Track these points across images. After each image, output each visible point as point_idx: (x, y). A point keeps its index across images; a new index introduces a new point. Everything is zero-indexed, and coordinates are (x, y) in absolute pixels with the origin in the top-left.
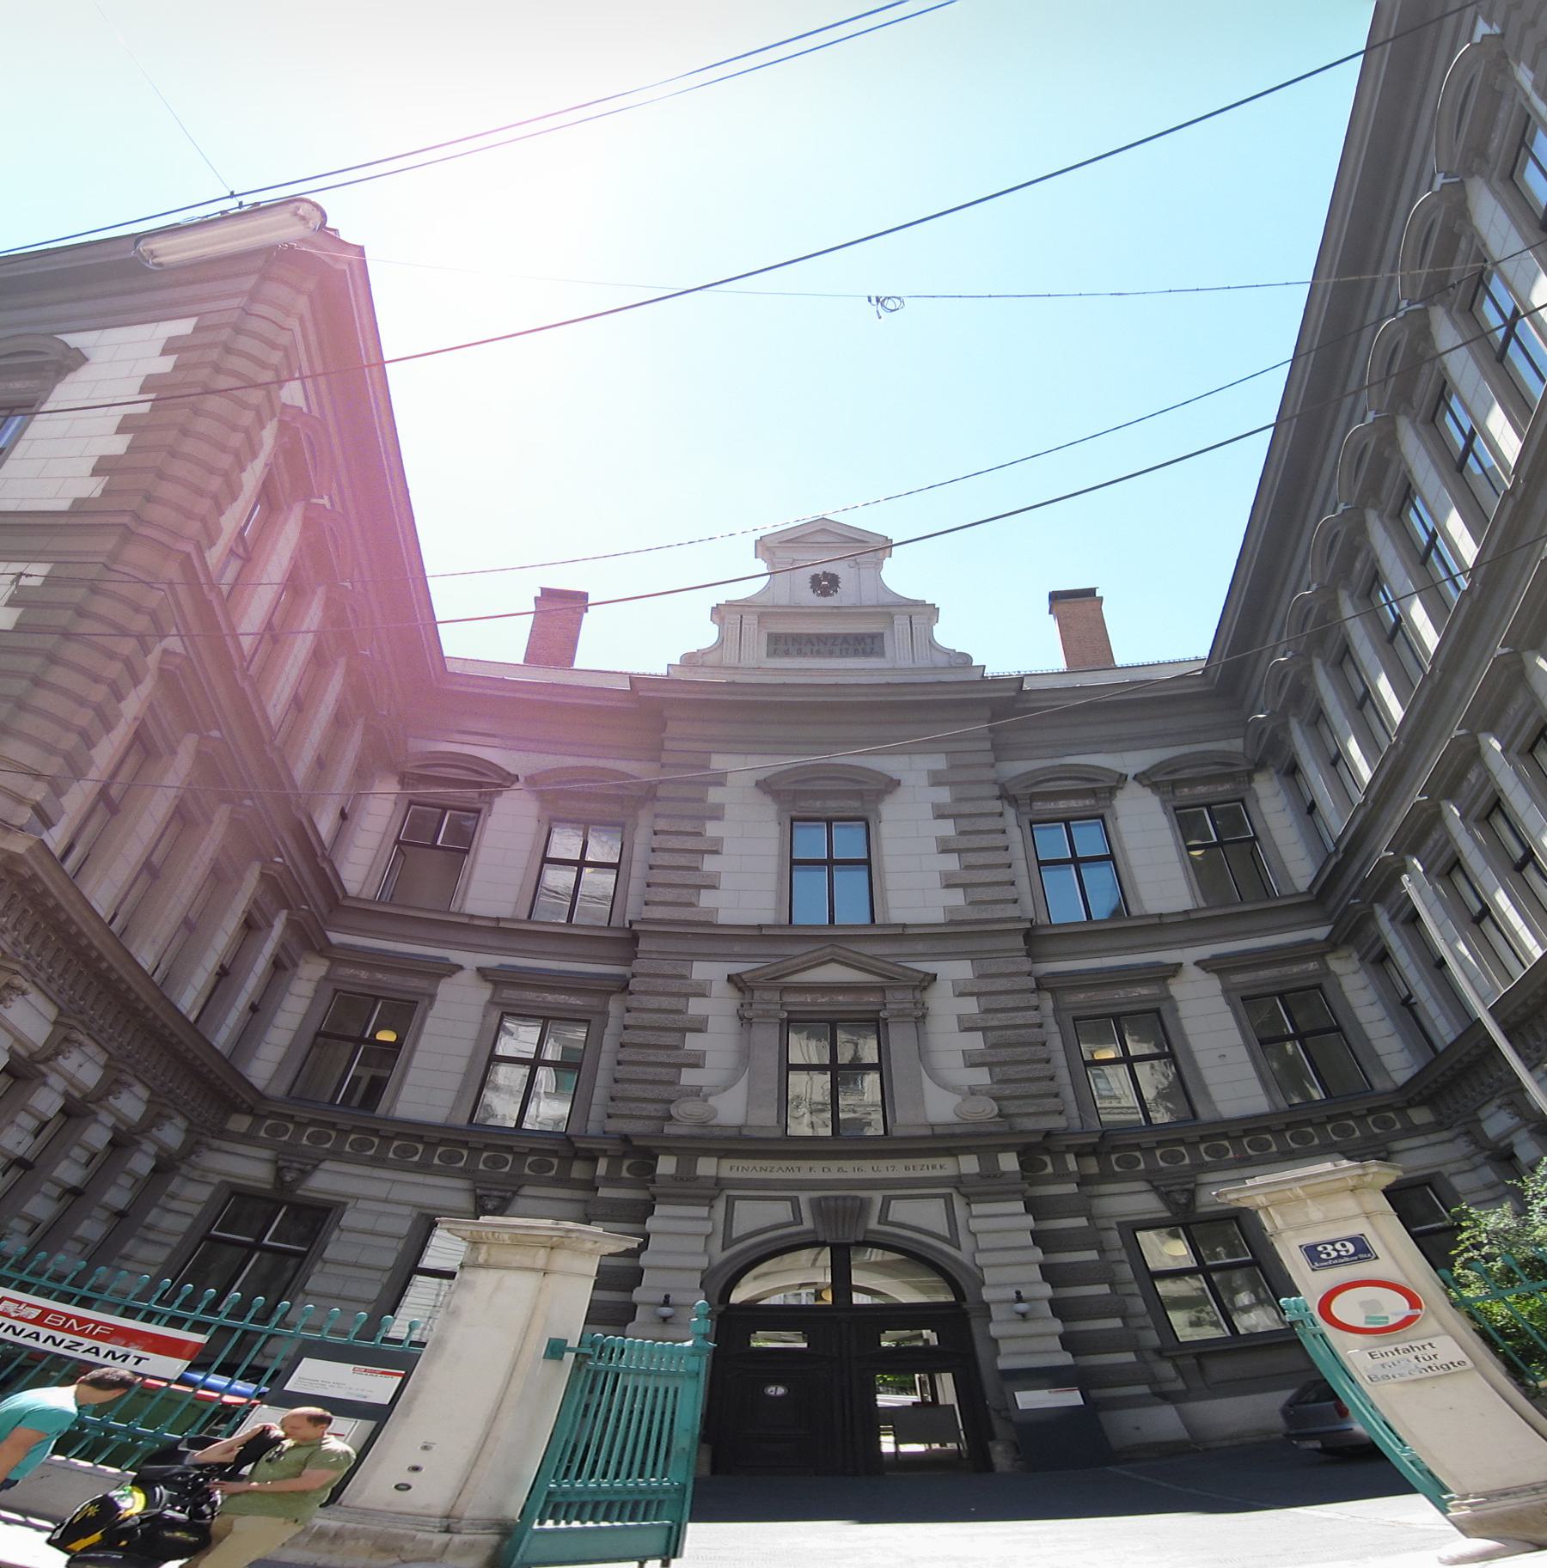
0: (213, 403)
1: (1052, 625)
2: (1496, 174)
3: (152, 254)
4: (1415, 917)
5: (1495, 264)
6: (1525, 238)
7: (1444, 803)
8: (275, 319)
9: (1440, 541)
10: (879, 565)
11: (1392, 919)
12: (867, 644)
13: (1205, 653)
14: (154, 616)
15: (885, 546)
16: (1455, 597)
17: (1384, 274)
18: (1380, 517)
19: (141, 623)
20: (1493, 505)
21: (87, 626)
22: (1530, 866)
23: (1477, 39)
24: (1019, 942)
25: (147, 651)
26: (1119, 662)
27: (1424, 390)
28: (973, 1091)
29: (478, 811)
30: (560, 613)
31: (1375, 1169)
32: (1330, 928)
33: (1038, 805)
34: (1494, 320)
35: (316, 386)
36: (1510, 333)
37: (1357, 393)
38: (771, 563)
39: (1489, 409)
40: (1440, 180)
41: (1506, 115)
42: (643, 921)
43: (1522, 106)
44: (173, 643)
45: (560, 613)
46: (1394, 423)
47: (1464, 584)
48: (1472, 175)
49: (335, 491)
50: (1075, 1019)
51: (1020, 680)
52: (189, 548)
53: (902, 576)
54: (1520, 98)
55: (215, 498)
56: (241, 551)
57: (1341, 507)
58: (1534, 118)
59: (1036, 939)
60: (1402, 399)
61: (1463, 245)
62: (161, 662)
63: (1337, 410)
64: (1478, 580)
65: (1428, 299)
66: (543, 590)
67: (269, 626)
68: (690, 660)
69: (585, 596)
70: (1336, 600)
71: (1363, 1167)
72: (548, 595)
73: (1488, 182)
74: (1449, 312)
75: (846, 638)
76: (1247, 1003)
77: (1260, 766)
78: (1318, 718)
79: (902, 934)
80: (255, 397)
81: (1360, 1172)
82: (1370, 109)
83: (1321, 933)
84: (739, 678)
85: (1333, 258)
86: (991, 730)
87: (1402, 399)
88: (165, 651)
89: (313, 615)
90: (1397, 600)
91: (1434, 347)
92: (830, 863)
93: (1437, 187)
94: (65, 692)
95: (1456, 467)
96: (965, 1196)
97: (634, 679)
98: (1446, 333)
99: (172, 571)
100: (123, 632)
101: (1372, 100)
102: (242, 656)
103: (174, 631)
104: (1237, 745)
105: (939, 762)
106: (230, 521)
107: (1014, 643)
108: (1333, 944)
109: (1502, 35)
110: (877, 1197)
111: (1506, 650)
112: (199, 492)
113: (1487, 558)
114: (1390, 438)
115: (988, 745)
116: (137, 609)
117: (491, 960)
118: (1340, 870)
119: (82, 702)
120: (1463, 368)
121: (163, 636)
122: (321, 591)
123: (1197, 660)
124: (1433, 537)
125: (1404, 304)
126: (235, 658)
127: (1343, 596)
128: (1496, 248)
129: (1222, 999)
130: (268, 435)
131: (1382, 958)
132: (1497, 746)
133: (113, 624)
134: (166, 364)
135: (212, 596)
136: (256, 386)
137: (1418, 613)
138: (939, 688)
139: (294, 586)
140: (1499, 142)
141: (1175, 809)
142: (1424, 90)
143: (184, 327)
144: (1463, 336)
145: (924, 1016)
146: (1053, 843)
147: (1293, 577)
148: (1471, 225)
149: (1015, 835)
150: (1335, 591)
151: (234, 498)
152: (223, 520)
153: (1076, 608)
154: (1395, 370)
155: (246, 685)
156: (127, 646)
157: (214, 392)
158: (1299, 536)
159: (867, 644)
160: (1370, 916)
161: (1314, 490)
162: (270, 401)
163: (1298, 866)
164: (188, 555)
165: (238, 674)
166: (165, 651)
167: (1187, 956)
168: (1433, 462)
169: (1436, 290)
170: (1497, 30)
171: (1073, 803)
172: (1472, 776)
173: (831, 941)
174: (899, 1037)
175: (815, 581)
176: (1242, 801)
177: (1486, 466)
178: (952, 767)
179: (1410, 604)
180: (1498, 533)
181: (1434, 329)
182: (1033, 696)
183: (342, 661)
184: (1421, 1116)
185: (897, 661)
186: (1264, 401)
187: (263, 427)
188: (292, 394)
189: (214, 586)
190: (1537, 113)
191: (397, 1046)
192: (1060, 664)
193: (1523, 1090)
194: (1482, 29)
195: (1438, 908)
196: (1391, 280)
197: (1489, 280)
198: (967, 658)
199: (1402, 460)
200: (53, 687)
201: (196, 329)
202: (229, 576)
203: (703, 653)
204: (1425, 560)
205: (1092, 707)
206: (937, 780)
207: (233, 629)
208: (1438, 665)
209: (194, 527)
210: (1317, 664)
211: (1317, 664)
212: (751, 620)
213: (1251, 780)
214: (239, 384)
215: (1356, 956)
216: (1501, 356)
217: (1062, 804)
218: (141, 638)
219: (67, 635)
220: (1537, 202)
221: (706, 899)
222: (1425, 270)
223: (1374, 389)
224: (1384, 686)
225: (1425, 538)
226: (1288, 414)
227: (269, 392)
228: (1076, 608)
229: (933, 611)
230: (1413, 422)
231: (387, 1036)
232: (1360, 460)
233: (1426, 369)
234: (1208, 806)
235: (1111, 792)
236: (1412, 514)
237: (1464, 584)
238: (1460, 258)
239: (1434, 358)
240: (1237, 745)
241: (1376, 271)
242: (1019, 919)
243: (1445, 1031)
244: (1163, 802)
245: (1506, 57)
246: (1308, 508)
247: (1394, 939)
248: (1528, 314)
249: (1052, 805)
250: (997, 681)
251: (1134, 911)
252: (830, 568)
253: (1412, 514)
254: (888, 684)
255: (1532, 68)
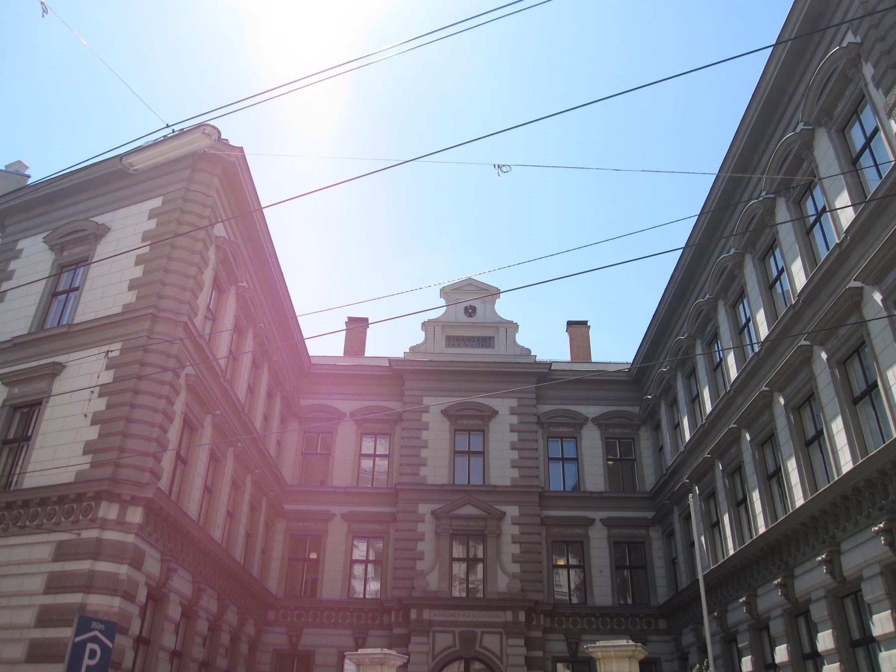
0: (180, 241)
1: (566, 338)
2: (835, 127)
3: (131, 165)
4: (689, 517)
5: (820, 179)
6: (841, 167)
7: (717, 461)
8: (201, 188)
9: (751, 324)
10: (494, 303)
11: (679, 516)
12: (486, 342)
13: (631, 361)
14: (177, 357)
15: (497, 293)
16: (751, 354)
17: (757, 175)
18: (725, 305)
19: (172, 363)
20: (782, 310)
21: (148, 371)
22: (743, 505)
23: (844, 44)
24: (536, 498)
25: (178, 377)
26: (593, 360)
27: (763, 242)
28: (514, 576)
29: (332, 433)
30: (357, 328)
31: (639, 649)
32: (653, 514)
33: (552, 429)
34: (810, 210)
35: (230, 225)
36: (818, 220)
37: (728, 238)
38: (447, 301)
39: (795, 259)
40: (801, 126)
41: (850, 93)
42: (400, 484)
43: (861, 89)
44: (189, 370)
45: (357, 328)
46: (744, 257)
47: (757, 349)
48: (820, 126)
49: (248, 278)
50: (553, 542)
51: (550, 364)
52: (186, 319)
53: (504, 308)
54: (862, 84)
55: (192, 291)
56: (210, 316)
57: (708, 296)
58: (867, 97)
59: (545, 497)
60: (750, 245)
61: (805, 165)
62: (186, 381)
63: (716, 245)
64: (764, 348)
65: (777, 193)
66: (349, 318)
67: (231, 352)
68: (413, 349)
69: (367, 319)
70: (695, 344)
71: (636, 646)
72: (352, 321)
73: (829, 132)
74: (787, 202)
75: (479, 338)
76: (615, 544)
77: (644, 423)
78: (673, 403)
79: (495, 490)
80: (201, 234)
81: (634, 648)
82: (770, 80)
83: (649, 515)
84: (434, 359)
85: (731, 162)
86: (536, 388)
87: (750, 245)
88: (187, 375)
89: (249, 344)
90: (722, 350)
91: (774, 220)
92: (563, 459)
93: (798, 130)
94: (148, 408)
95: (769, 286)
96: (507, 634)
97: (391, 360)
98: (783, 213)
99: (180, 333)
100: (165, 369)
101: (773, 74)
102: (222, 370)
103: (188, 364)
104: (636, 410)
105: (514, 403)
106: (202, 301)
107: (549, 346)
108: (653, 522)
109: (861, 44)
110: (479, 631)
111: (767, 389)
112: (184, 289)
113: (772, 338)
114: (739, 265)
115: (534, 396)
116: (169, 356)
117: (346, 509)
118: (666, 483)
119: (156, 410)
120: (787, 234)
121: (184, 367)
122: (251, 330)
123: (627, 363)
124: (748, 320)
125: (764, 193)
126: (219, 372)
127: (699, 343)
128: (823, 171)
129: (606, 541)
130: (212, 254)
131: (670, 535)
132: (748, 437)
133: (160, 367)
134: (152, 224)
135: (202, 342)
136: (200, 229)
137: (731, 359)
138: (516, 366)
139: (238, 330)
140: (841, 109)
141: (606, 438)
142: (805, 72)
143: (157, 202)
144: (791, 216)
145: (500, 534)
146: (555, 449)
147: (677, 328)
148: (812, 155)
149: (541, 443)
150: (695, 340)
151: (201, 289)
152: (198, 301)
153: (578, 330)
154: (751, 228)
155: (226, 384)
156: (169, 376)
157: (179, 235)
158: (684, 308)
159: (486, 342)
160: (671, 512)
161: (696, 285)
162: (209, 235)
163: (649, 478)
164: (186, 323)
165: (222, 379)
166: (187, 375)
167: (598, 515)
168: (758, 281)
169: (784, 188)
170: (858, 40)
171: (566, 430)
172: (733, 450)
173: (468, 493)
174: (491, 542)
175: (466, 309)
176: (633, 439)
177: (785, 289)
178: (520, 406)
179: (729, 353)
180: (781, 326)
181: (777, 210)
182: (555, 373)
183: (266, 365)
184: (662, 624)
185: (496, 354)
186: (681, 235)
187: (208, 250)
188: (219, 230)
189: (201, 337)
190: (870, 96)
191: (317, 561)
192: (568, 358)
193: (702, 624)
194: (850, 38)
195: (699, 515)
196: (760, 179)
197: (814, 188)
198: (529, 351)
199: (743, 277)
200: (141, 406)
201: (164, 203)
202: (207, 330)
203: (418, 346)
204: (741, 332)
205: (578, 381)
206: (513, 412)
207: (214, 356)
208: (733, 388)
209: (185, 308)
210: (679, 375)
211: (679, 375)
212: (438, 329)
213: (639, 430)
214: (192, 229)
215: (661, 531)
216: (809, 231)
217: (561, 430)
218: (174, 370)
219: (139, 378)
220: (854, 147)
221: (423, 471)
222: (780, 177)
223: (738, 237)
224: (706, 393)
225: (744, 321)
226: (691, 243)
227: (207, 231)
228: (578, 330)
229: (514, 327)
230: (753, 258)
231: (313, 556)
232: (722, 273)
233: (767, 230)
234: (619, 439)
235: (581, 425)
236: (741, 307)
237: (757, 349)
238: (801, 172)
239: (773, 226)
240: (636, 410)
241: (753, 173)
242: (537, 487)
243: (684, 581)
244: (602, 434)
245: (860, 58)
246: (691, 294)
247: (677, 527)
248: (831, 211)
249: (556, 430)
250: (541, 363)
251: (582, 489)
252: (472, 303)
253: (741, 307)
254: (495, 362)
255: (875, 67)
